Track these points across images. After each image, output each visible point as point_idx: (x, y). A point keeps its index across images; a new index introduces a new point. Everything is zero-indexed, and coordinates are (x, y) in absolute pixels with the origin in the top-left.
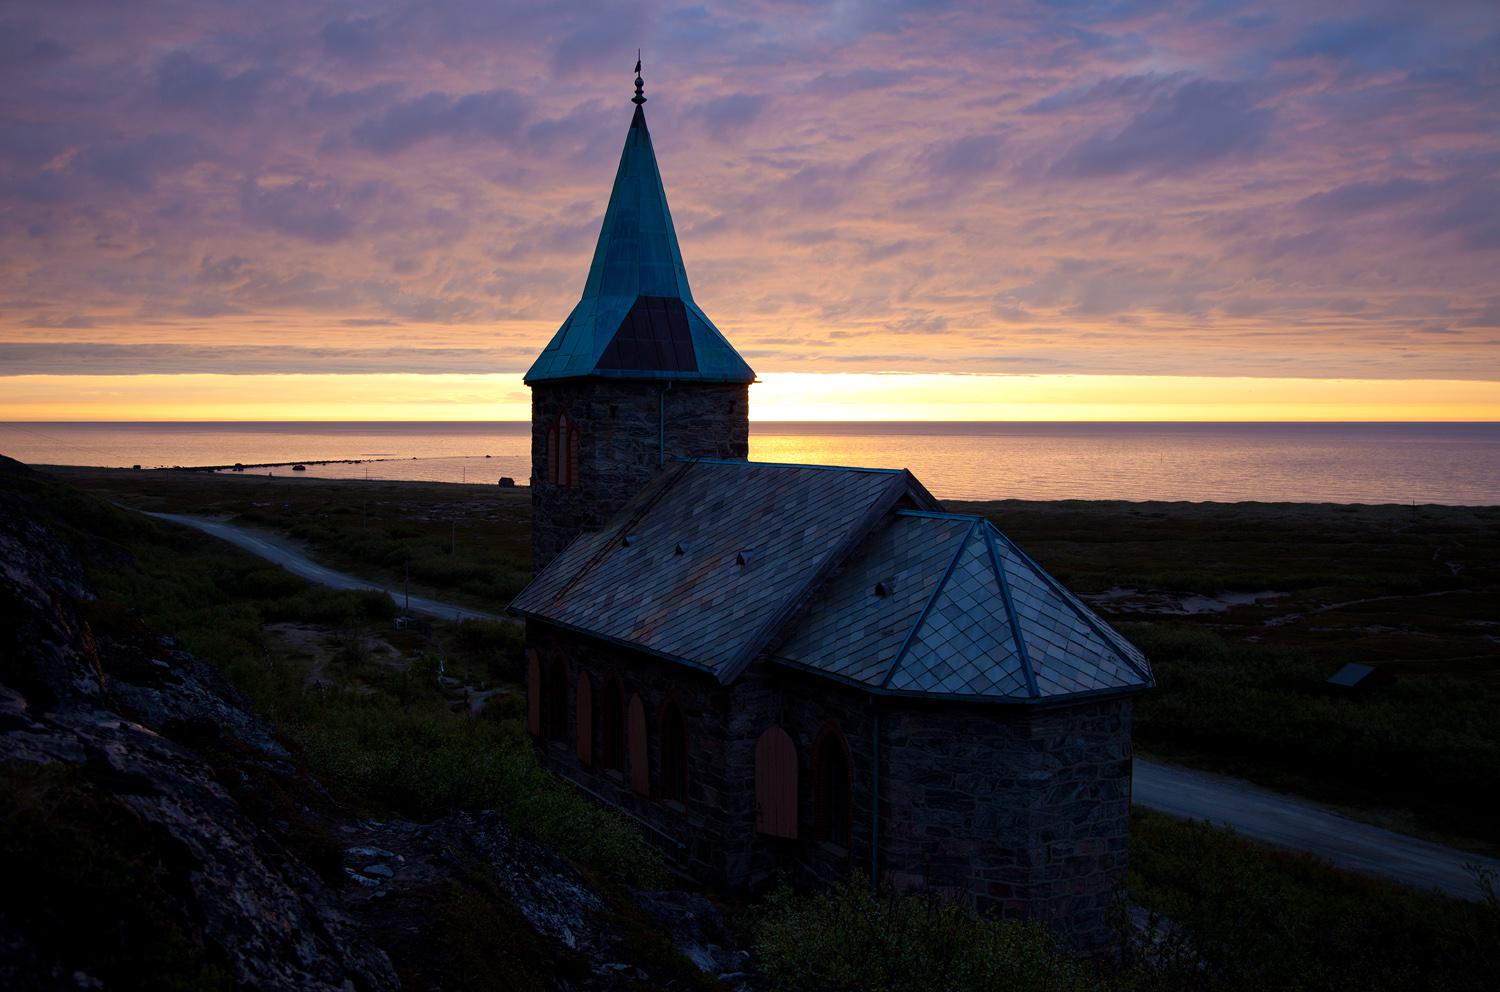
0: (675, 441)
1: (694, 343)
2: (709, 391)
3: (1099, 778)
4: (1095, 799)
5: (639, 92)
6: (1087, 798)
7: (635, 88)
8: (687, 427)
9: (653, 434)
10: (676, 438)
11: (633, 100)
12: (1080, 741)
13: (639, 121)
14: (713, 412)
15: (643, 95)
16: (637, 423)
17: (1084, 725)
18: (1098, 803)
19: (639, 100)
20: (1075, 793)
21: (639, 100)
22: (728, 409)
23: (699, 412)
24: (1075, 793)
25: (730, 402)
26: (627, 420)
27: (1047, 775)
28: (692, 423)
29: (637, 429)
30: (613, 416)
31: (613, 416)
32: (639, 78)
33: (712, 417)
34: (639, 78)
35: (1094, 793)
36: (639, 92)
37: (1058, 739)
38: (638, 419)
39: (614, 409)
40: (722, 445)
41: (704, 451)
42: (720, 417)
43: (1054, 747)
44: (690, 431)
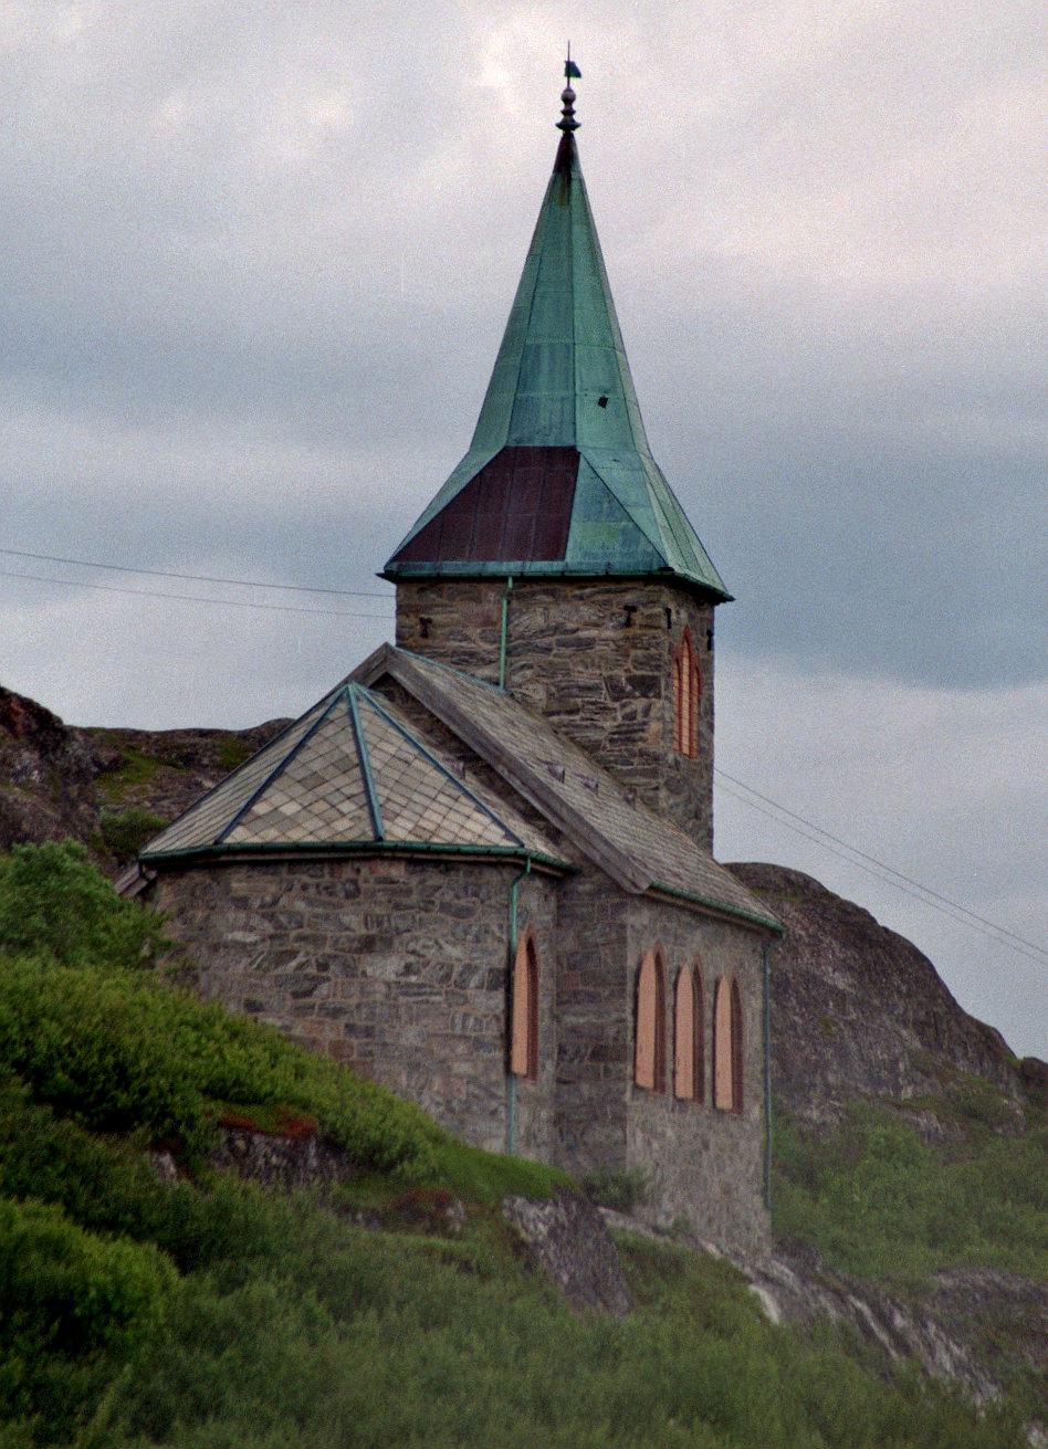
0: (528, 673)
1: (574, 516)
2: (588, 591)
3: (328, 950)
4: (324, 974)
5: (568, 112)
6: (312, 970)
7: (562, 106)
8: (550, 650)
9: (490, 662)
10: (531, 667)
11: (560, 126)
12: (300, 906)
13: (566, 158)
14: (596, 625)
15: (575, 117)
16: (464, 644)
17: (304, 887)
18: (328, 979)
19: (568, 126)
20: (294, 964)
21: (568, 126)
22: (622, 620)
23: (570, 626)
24: (294, 964)
25: (626, 608)
26: (448, 639)
27: (251, 938)
28: (561, 644)
29: (465, 653)
30: (425, 635)
31: (425, 635)
32: (568, 90)
33: (593, 633)
34: (568, 90)
35: (323, 967)
36: (568, 112)
37: (268, 899)
38: (466, 638)
39: (425, 623)
40: (611, 678)
41: (579, 687)
42: (609, 634)
43: (262, 906)
44: (555, 656)
